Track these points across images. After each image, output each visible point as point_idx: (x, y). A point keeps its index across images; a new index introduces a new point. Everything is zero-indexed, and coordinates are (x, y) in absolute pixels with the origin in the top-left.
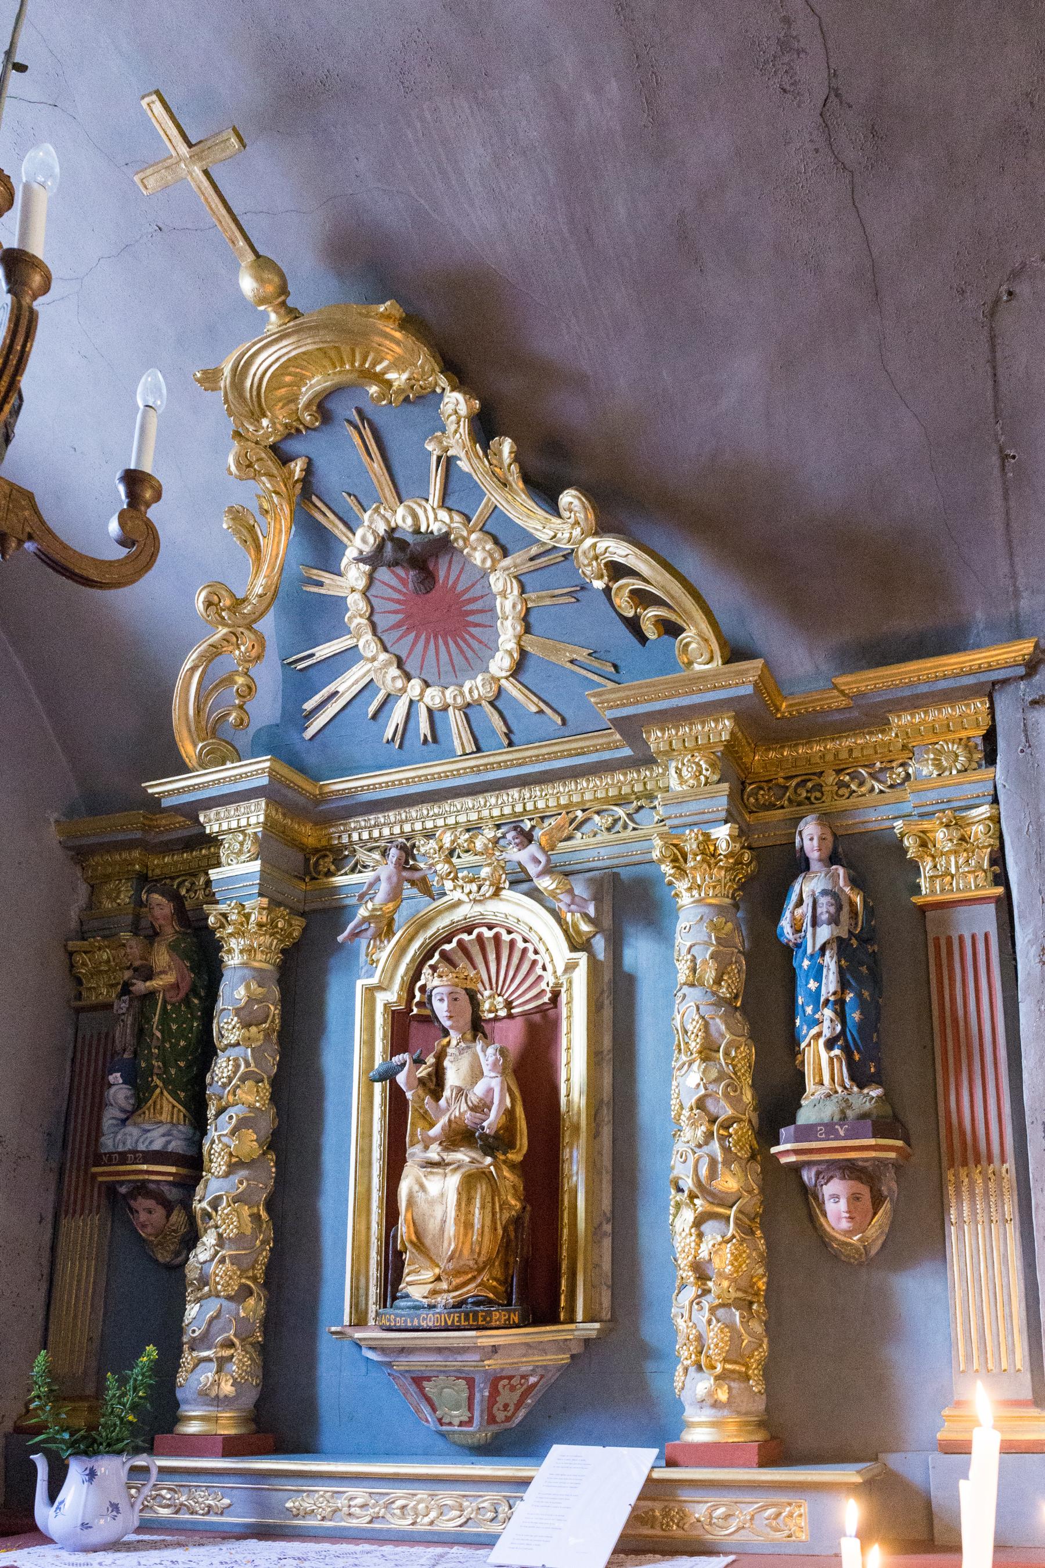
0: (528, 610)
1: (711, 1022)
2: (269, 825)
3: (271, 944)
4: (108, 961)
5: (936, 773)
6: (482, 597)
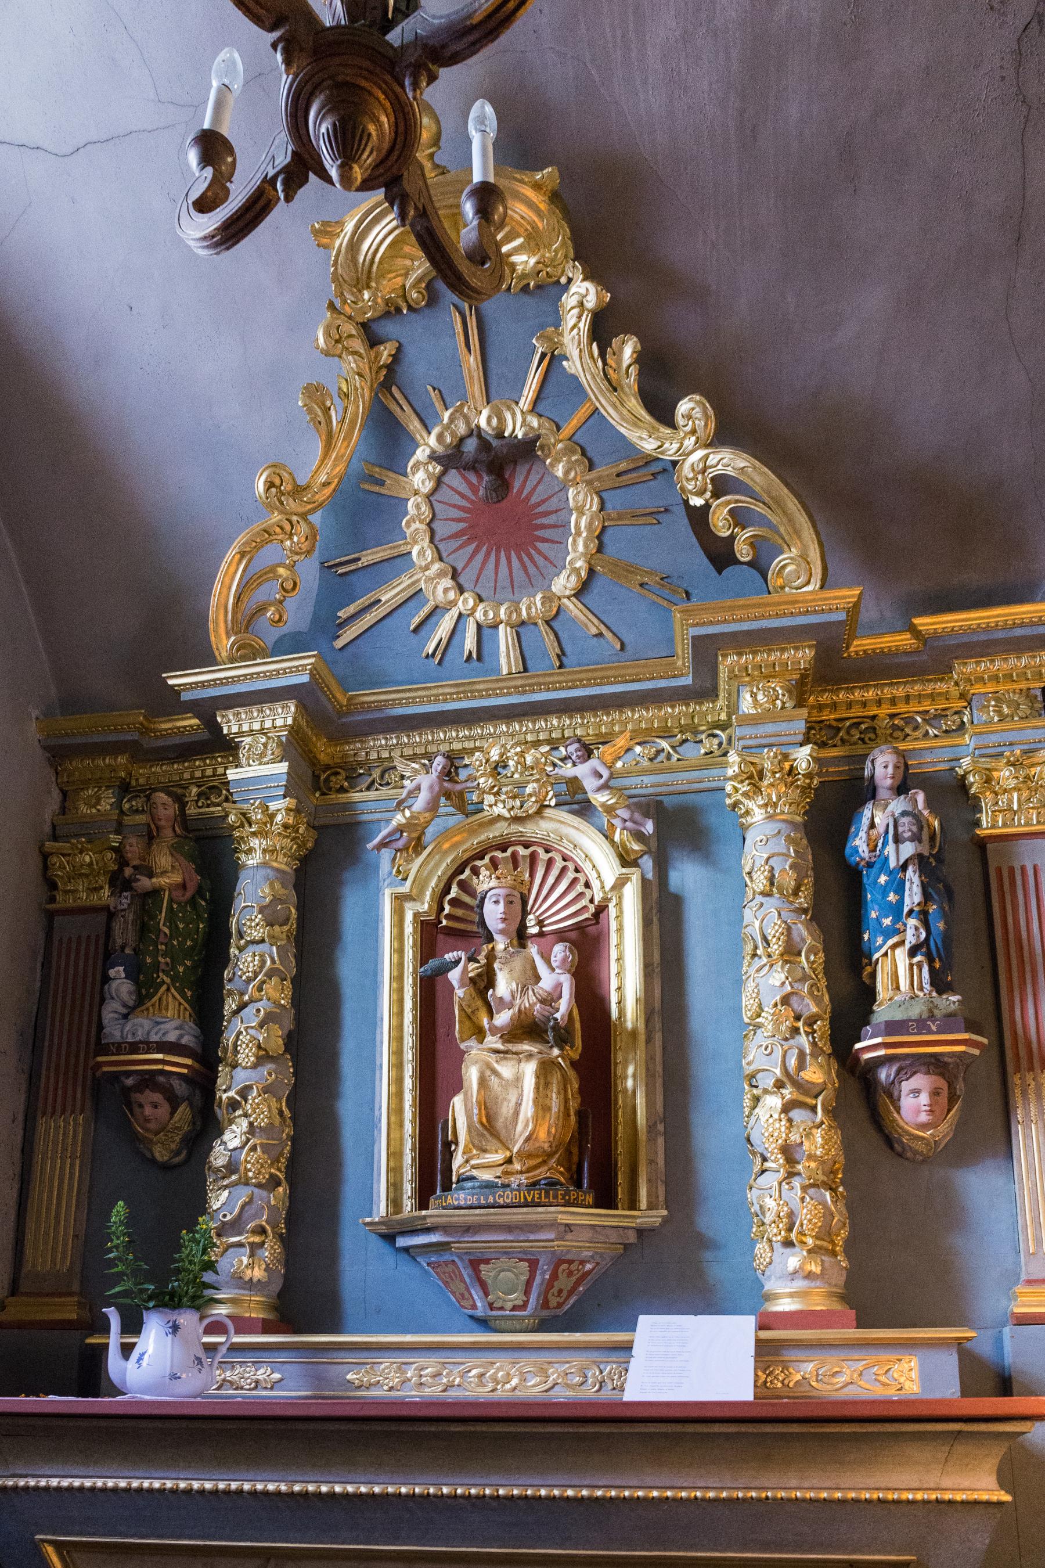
0: (604, 528)
1: (793, 927)
2: (294, 730)
3: (291, 848)
4: (91, 864)
5: (996, 719)
6: (556, 511)
